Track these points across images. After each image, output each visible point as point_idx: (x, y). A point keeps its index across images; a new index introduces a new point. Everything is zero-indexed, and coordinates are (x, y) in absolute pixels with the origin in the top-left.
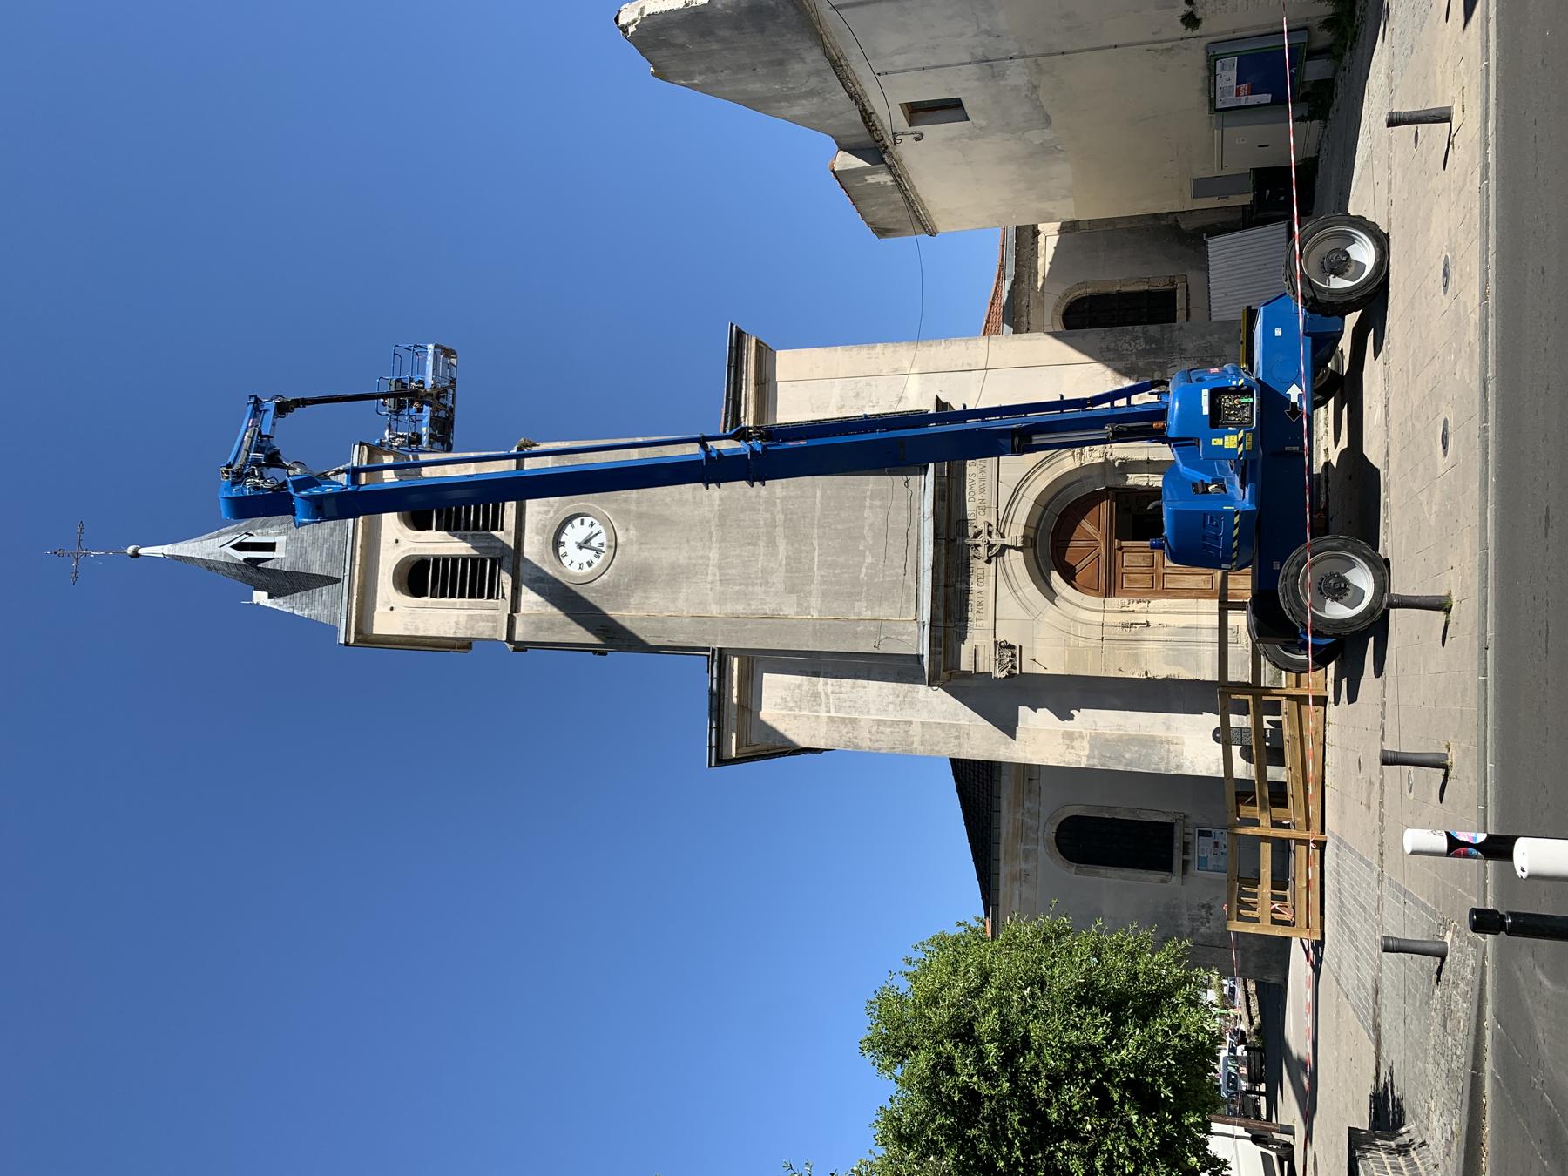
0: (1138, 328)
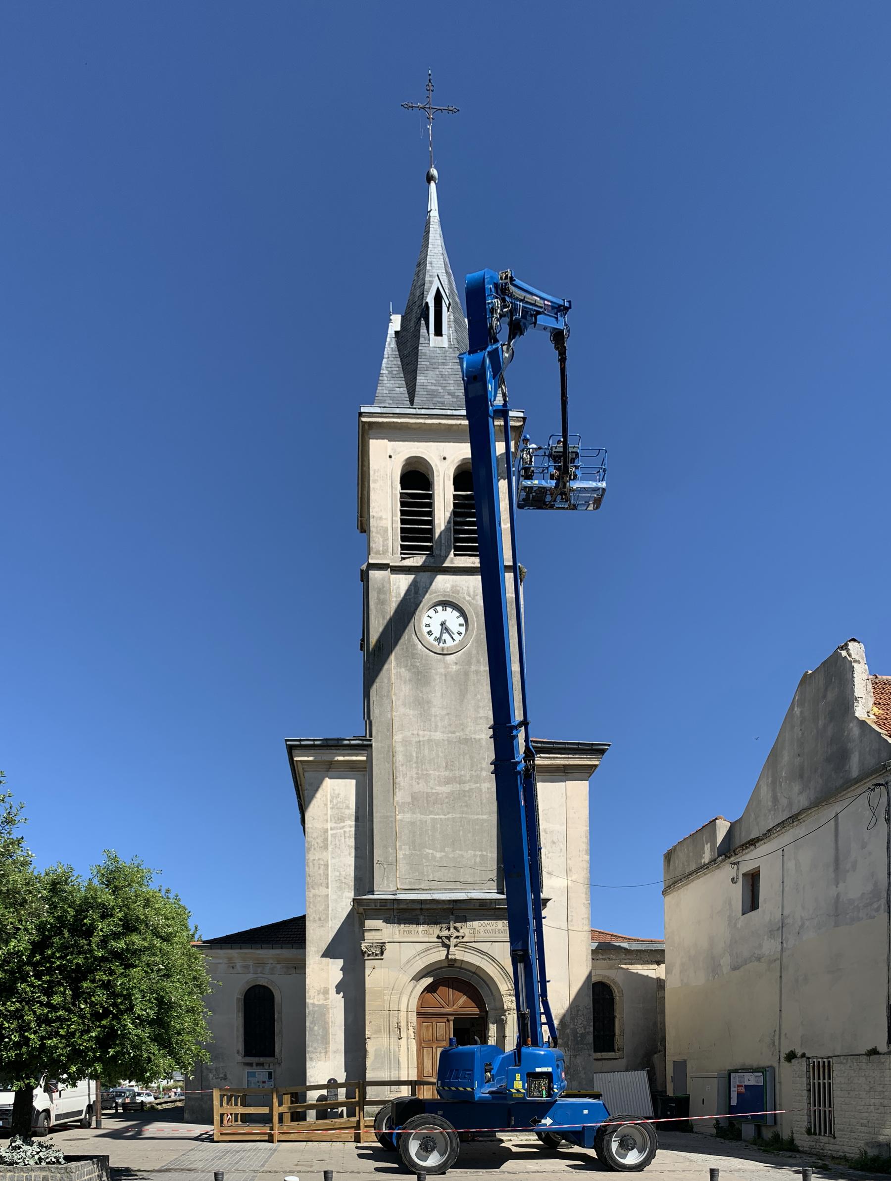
0: (592, 1029)
